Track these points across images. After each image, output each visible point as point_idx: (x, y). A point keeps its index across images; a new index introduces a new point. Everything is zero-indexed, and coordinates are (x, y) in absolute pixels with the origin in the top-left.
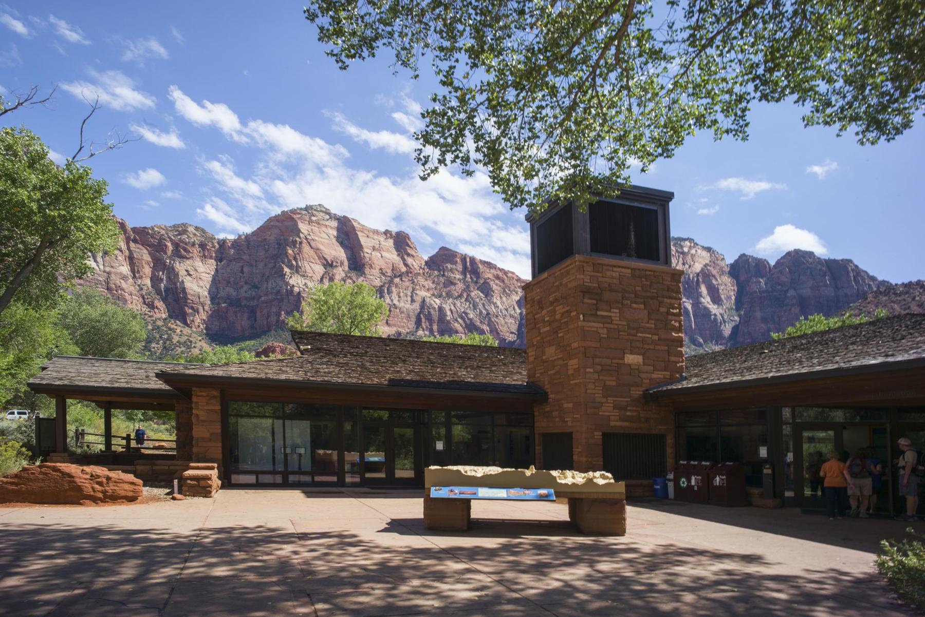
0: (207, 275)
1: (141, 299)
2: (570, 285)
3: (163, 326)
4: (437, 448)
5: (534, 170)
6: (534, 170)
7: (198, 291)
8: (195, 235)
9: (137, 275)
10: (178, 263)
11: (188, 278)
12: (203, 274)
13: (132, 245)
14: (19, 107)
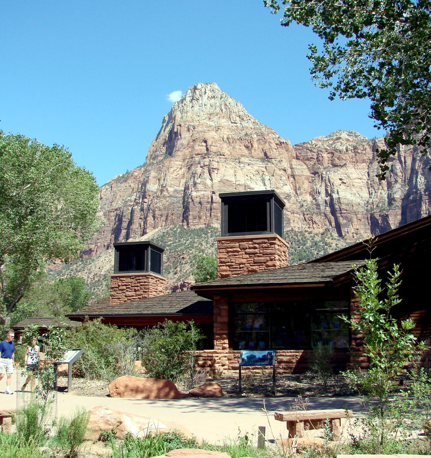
0: (359, 181)
1: (302, 216)
2: (150, 295)
3: (320, 241)
4: (263, 343)
5: (409, 135)
6: (409, 135)
7: (351, 198)
8: (348, 140)
9: (298, 192)
10: (333, 174)
11: (343, 186)
12: (355, 181)
13: (294, 162)
14: (5, 395)
